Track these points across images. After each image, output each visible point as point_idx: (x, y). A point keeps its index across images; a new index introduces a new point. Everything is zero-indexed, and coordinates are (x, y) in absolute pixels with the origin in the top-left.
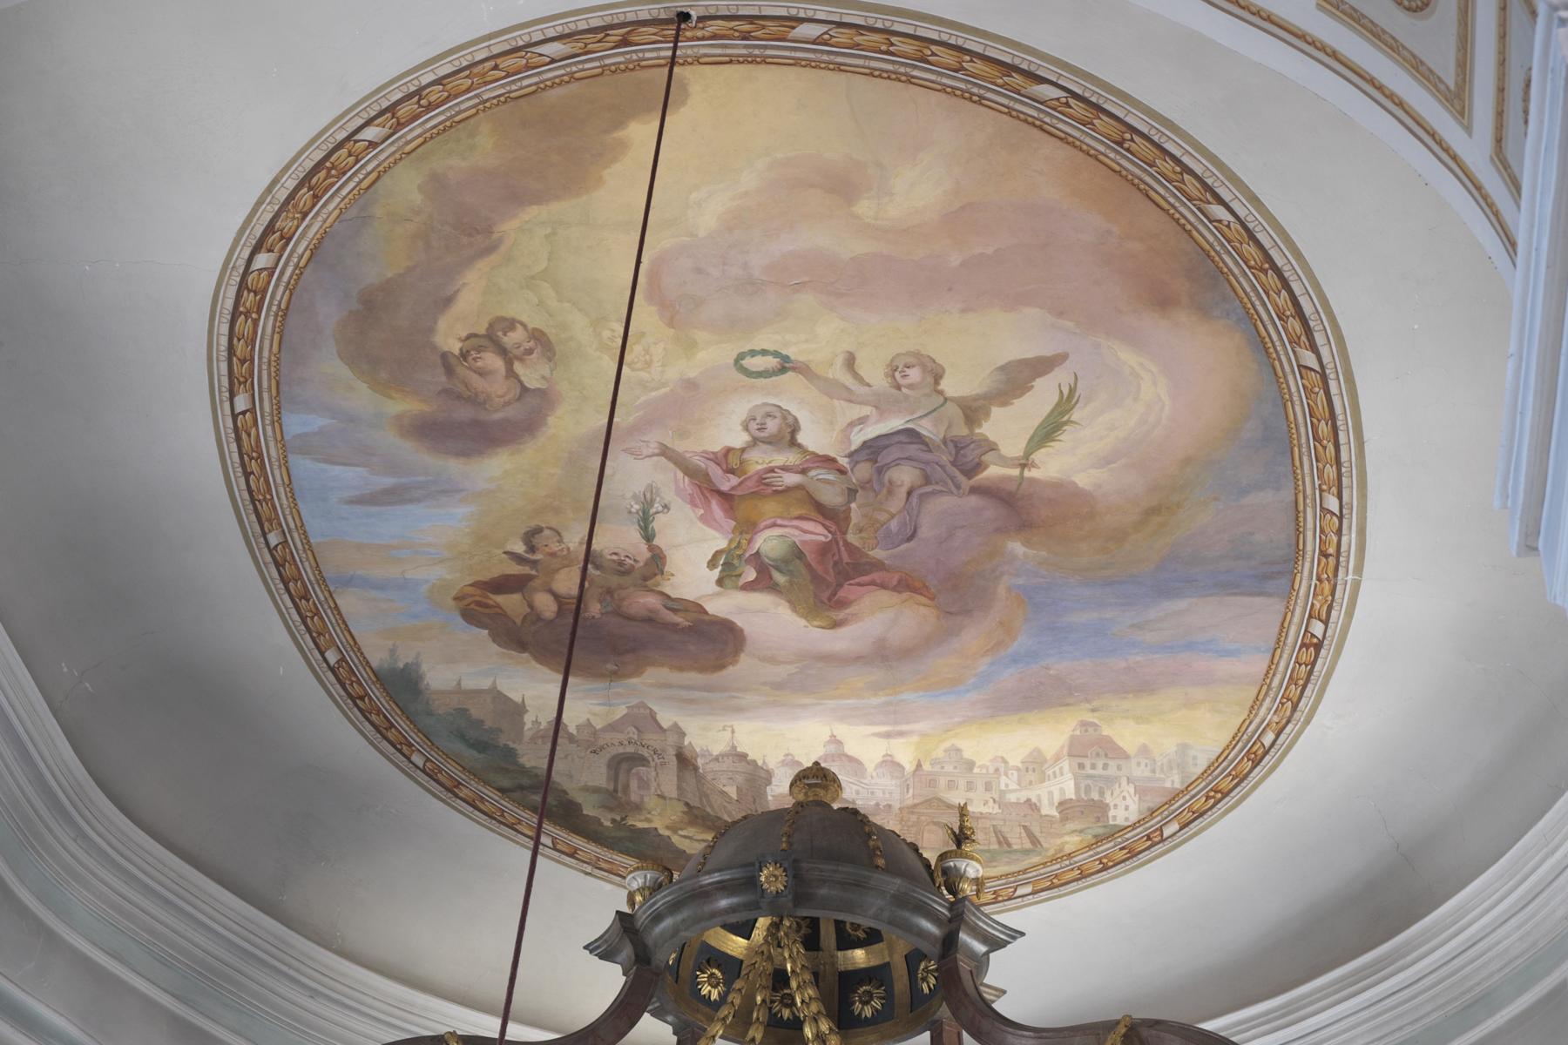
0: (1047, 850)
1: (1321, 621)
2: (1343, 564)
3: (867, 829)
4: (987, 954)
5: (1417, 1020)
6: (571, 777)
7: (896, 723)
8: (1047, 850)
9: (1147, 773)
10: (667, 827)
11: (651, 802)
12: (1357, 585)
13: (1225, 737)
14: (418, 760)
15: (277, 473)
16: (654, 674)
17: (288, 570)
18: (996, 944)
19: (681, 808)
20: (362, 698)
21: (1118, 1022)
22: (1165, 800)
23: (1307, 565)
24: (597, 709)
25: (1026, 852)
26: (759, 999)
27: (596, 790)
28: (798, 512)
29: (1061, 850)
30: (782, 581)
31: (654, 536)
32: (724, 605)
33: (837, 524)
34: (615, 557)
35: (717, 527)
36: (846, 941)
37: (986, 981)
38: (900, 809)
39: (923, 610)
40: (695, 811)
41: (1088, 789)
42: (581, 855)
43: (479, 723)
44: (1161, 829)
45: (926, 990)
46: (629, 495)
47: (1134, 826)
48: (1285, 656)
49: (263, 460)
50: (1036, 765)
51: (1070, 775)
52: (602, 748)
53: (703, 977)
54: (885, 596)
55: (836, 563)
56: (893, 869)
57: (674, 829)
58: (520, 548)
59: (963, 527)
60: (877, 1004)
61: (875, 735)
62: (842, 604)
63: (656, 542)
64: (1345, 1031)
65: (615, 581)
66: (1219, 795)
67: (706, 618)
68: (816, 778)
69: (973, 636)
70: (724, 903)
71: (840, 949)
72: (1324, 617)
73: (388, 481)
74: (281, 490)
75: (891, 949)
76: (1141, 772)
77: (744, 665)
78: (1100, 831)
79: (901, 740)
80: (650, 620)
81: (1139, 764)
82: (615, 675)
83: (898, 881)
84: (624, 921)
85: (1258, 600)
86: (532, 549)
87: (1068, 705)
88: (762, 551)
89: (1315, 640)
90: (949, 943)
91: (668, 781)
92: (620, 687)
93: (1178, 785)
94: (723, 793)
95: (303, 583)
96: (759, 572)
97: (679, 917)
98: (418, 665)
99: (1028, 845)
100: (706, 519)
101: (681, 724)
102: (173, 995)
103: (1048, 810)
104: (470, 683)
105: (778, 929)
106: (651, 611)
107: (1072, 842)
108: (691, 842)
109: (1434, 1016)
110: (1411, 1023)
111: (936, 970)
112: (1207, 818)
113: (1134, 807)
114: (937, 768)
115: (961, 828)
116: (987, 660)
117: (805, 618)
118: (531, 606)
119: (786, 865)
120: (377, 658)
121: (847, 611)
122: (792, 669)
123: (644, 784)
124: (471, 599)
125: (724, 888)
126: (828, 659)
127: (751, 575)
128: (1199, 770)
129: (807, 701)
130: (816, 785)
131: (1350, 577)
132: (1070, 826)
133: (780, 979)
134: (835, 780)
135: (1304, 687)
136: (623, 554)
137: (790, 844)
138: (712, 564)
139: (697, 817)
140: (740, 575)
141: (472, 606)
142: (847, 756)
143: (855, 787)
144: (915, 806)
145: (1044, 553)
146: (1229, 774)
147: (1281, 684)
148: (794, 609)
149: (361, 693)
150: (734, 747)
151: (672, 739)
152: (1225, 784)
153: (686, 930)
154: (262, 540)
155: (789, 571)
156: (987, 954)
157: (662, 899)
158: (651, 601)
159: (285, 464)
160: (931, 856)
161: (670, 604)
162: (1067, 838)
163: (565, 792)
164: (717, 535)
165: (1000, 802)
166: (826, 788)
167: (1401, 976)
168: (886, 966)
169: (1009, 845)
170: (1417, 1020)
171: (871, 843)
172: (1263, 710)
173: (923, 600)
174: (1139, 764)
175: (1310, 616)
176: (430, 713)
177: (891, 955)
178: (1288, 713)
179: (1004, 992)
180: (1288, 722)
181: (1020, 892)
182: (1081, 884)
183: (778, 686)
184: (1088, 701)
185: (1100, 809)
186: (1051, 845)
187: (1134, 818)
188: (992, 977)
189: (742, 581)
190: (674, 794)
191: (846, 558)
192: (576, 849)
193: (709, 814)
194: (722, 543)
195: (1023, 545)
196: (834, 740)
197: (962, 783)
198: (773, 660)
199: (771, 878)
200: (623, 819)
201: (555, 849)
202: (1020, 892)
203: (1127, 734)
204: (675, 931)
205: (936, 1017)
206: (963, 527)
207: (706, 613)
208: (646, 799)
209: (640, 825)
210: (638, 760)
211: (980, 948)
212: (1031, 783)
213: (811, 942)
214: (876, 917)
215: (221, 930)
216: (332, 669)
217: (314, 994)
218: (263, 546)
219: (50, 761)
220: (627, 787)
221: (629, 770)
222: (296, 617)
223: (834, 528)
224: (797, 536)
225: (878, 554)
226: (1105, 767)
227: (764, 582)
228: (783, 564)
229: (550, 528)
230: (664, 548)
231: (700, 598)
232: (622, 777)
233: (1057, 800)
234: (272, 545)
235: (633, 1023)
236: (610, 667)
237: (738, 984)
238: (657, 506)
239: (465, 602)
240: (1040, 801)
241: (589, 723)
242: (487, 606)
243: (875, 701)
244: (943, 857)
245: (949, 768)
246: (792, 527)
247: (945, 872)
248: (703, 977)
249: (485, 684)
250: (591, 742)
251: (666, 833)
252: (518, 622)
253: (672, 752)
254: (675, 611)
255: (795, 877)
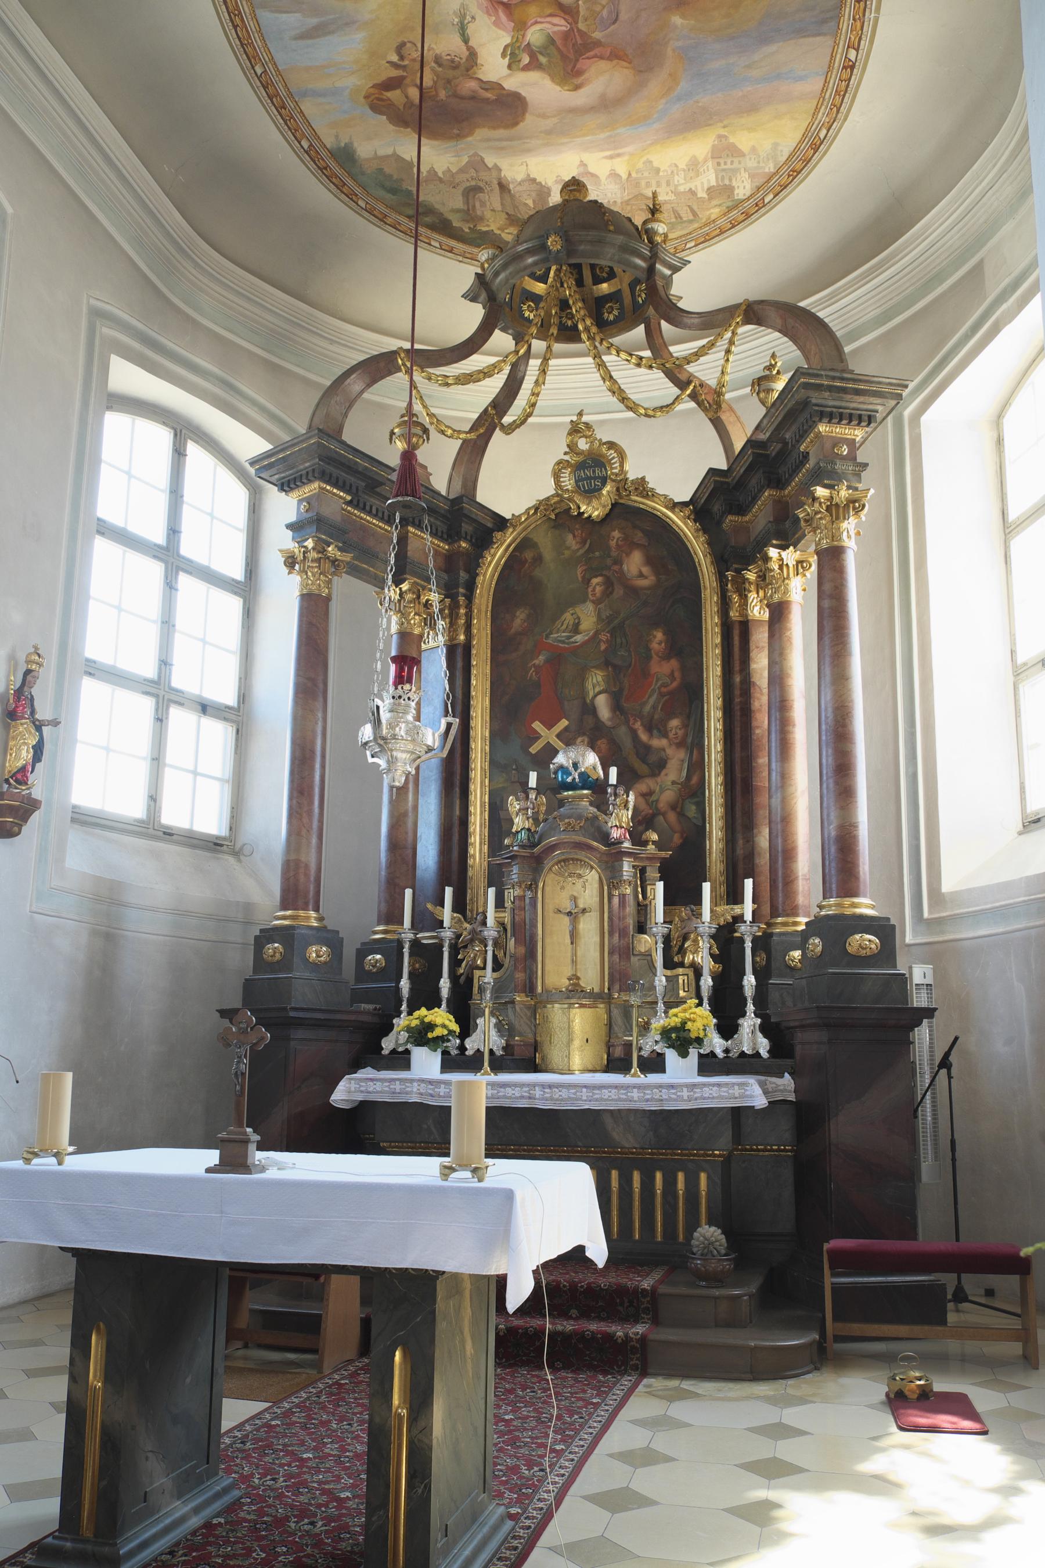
0: (702, 219)
1: (854, 49)
2: (869, 6)
3: (603, 210)
4: (671, 275)
5: (900, 293)
6: (444, 204)
7: (616, 148)
8: (702, 219)
9: (755, 165)
10: (499, 229)
11: (488, 214)
12: (877, 19)
13: (798, 136)
14: (361, 203)
15: (251, 23)
16: (481, 133)
17: (271, 90)
18: (676, 269)
19: (504, 216)
20: (326, 168)
21: (741, 304)
22: (765, 180)
23: (847, 10)
24: (453, 159)
25: (690, 222)
26: (553, 312)
27: (458, 211)
28: (549, 11)
29: (709, 219)
30: (799, 1034)
31: (469, 40)
32: (514, 82)
33: (572, 17)
34: (449, 57)
35: (504, 29)
36: (598, 281)
37: (672, 292)
38: (622, 203)
39: (626, 71)
40: (513, 218)
41: (723, 178)
42: (455, 251)
43: (391, 176)
44: (763, 199)
45: (641, 302)
46: (451, 12)
47: (748, 199)
48: (833, 76)
49: (242, 16)
50: (694, 167)
51: (713, 171)
52: (458, 184)
53: (525, 307)
54: (603, 64)
55: (573, 45)
56: (619, 230)
57: (502, 229)
58: (395, 58)
59: (645, 9)
60: (616, 312)
61: (606, 157)
62: (579, 73)
63: (471, 43)
64: (862, 304)
65: (451, 74)
66: (795, 174)
67: (505, 92)
68: (574, 186)
69: (655, 86)
70: (530, 260)
71: (594, 284)
72: (856, 46)
73: (314, 21)
74: (256, 35)
75: (621, 281)
76: (751, 163)
77: (529, 121)
78: (730, 204)
79: (619, 160)
80: (473, 98)
81: (750, 159)
82: (459, 137)
83: (621, 237)
84: (480, 278)
85: (818, 39)
86: (402, 58)
87: (710, 125)
88: (531, 42)
89: (851, 63)
90: (651, 270)
91: (494, 200)
92: (462, 144)
93: (772, 170)
94: (526, 204)
95: (280, 97)
96: (530, 57)
97: (508, 272)
98: (352, 143)
99: (691, 217)
100: (497, 24)
101: (499, 164)
102: (262, 349)
103: (702, 194)
104: (381, 152)
105: (560, 272)
106: (474, 92)
107: (715, 212)
108: (508, 235)
109: (910, 289)
110: (897, 296)
111: (645, 289)
112: (789, 189)
113: (748, 186)
114: (640, 175)
115: (654, 205)
116: (663, 101)
117: (560, 85)
118: (407, 97)
119: (561, 234)
120: (329, 142)
121: (583, 78)
122: (555, 120)
123: (483, 204)
124: (373, 97)
125: (529, 252)
126: (574, 111)
127: (526, 60)
128: (784, 159)
129: (566, 140)
130: (574, 190)
131: (873, 15)
132: (715, 202)
133: (564, 305)
134: (584, 186)
135: (844, 96)
136: (453, 55)
137: (562, 223)
138: (503, 55)
139: (513, 220)
140: (520, 61)
141: (375, 101)
142: (590, 173)
143: (596, 192)
144: (630, 199)
145: (693, 22)
146: (801, 159)
147: (831, 95)
148: (553, 80)
149: (325, 165)
150: (528, 175)
151: (494, 174)
152: (798, 167)
153: (512, 278)
154: (252, 71)
155: (548, 54)
156: (671, 275)
157: (498, 263)
158: (472, 85)
159: (255, 17)
160: (638, 221)
161: (484, 86)
162: (712, 211)
163: (442, 214)
164: (504, 34)
165: (676, 193)
166: (579, 191)
167: (893, 269)
168: (619, 291)
169: (681, 218)
170: (900, 293)
171: (606, 218)
172: (820, 114)
173: (625, 64)
174: (750, 159)
175: (848, 47)
176: (363, 174)
177: (621, 285)
178: (834, 115)
179: (681, 298)
180: (834, 121)
181: (688, 246)
182: (721, 237)
183: (549, 132)
184: (721, 121)
185: (729, 190)
186: (704, 216)
187: (748, 194)
188: (674, 291)
189: (522, 65)
190: (500, 209)
191: (579, 41)
192: (452, 248)
193: (519, 219)
194: (507, 40)
195: (680, 17)
196: (583, 164)
197: (654, 183)
198: (544, 116)
199: (554, 243)
200: (475, 226)
201: (441, 249)
202: (688, 246)
203: (743, 140)
204: (507, 280)
205: (646, 316)
206: (645, 9)
207: (504, 89)
208: (485, 213)
209: (485, 229)
210: (477, 189)
211: (668, 272)
212: (691, 178)
213: (580, 283)
214: (611, 259)
215: (278, 311)
216: (306, 152)
217: (332, 342)
218: (254, 75)
219: (171, 224)
220: (474, 206)
221: (474, 196)
222: (281, 121)
223: (570, 20)
224: (550, 29)
225: (597, 35)
226: (732, 163)
227: (534, 65)
228: (544, 50)
229: (410, 42)
230: (475, 47)
231: (500, 79)
232: (471, 201)
233: (706, 188)
234: (259, 74)
235: (491, 334)
236: (456, 131)
237: (542, 305)
238: (468, 18)
239: (370, 99)
240: (696, 189)
241: (449, 170)
242: (382, 100)
243: (602, 136)
244: (645, 223)
245: (646, 174)
246: (547, 22)
247: (647, 231)
248: (525, 307)
249: (389, 151)
250: (450, 181)
251: (498, 232)
252: (401, 108)
253: (496, 182)
254: (486, 90)
255: (566, 240)
